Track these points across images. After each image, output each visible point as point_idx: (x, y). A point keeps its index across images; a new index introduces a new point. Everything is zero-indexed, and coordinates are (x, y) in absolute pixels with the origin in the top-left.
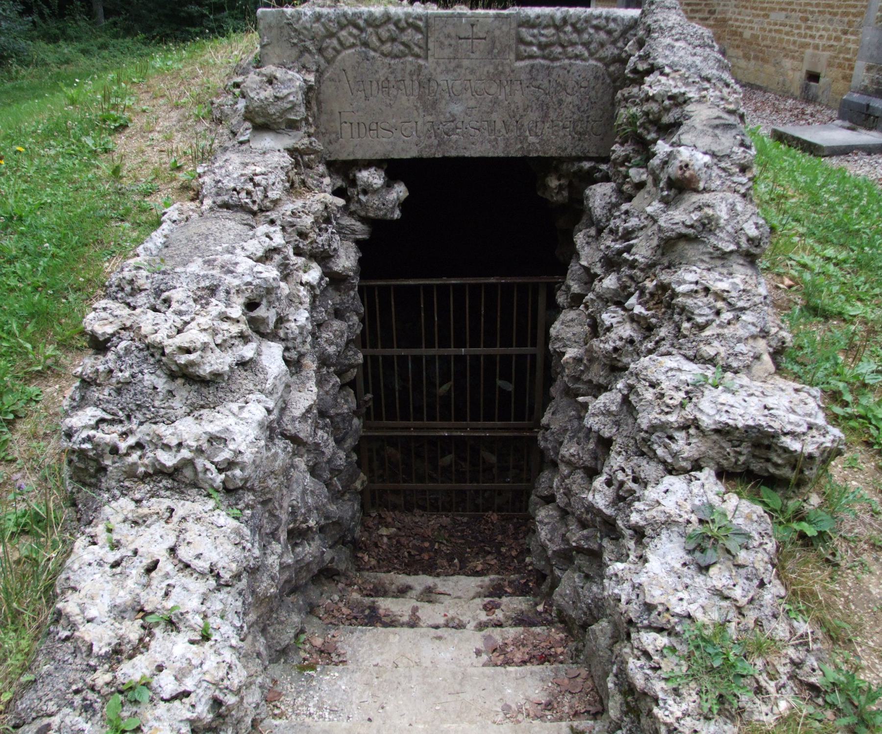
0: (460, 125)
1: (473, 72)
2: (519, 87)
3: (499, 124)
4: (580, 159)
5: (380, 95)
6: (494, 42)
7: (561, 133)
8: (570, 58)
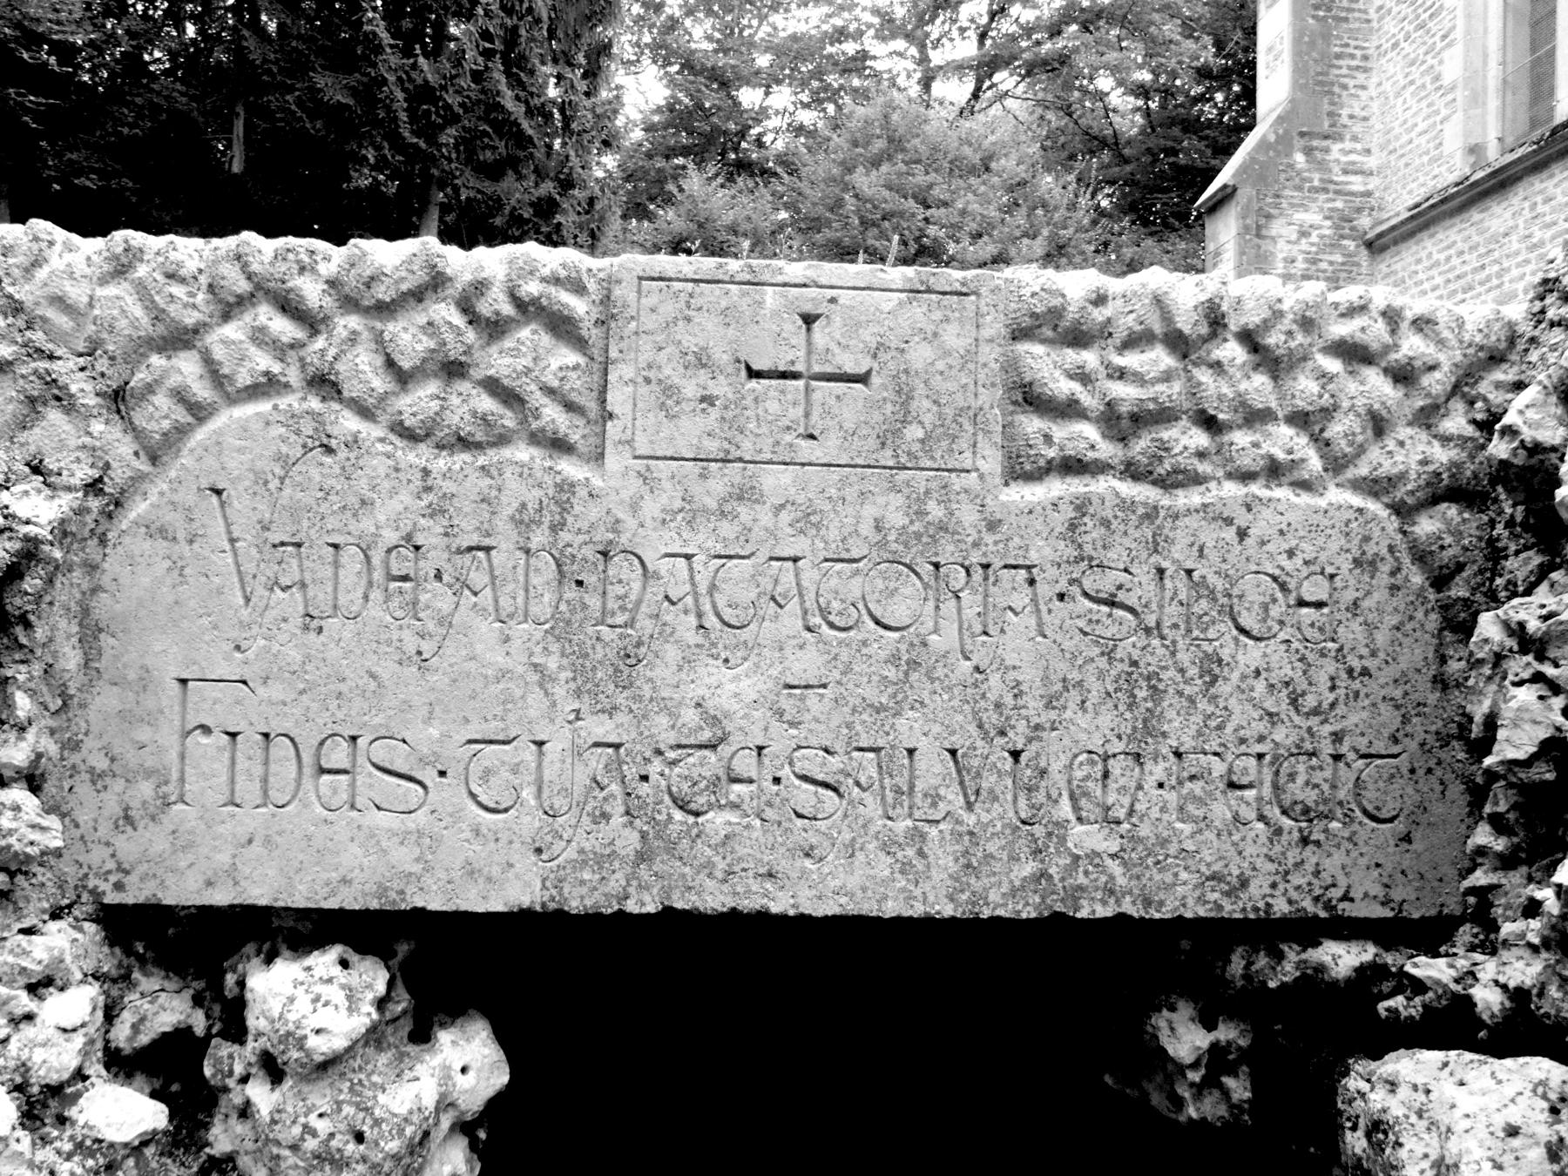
0: (745, 764)
1: (808, 521)
2: (1021, 599)
3: (932, 768)
4: (1308, 931)
5: (375, 611)
6: (905, 397)
7: (1220, 811)
8: (1246, 477)
